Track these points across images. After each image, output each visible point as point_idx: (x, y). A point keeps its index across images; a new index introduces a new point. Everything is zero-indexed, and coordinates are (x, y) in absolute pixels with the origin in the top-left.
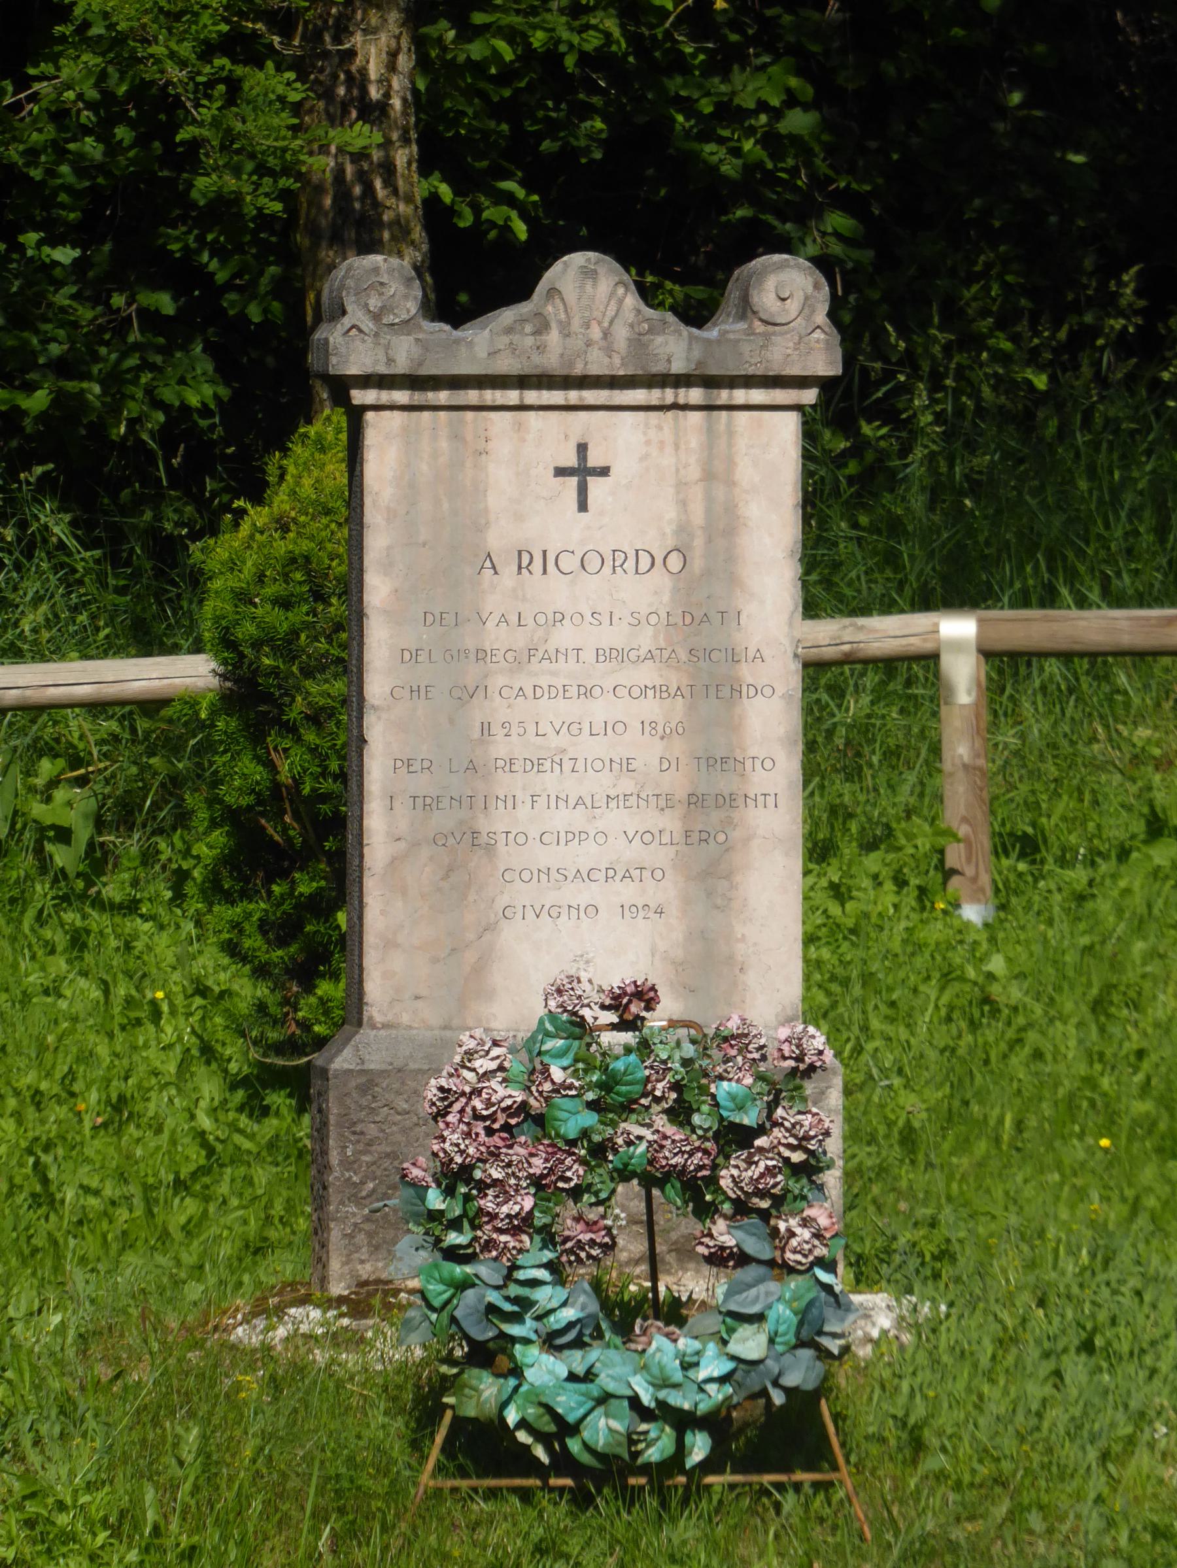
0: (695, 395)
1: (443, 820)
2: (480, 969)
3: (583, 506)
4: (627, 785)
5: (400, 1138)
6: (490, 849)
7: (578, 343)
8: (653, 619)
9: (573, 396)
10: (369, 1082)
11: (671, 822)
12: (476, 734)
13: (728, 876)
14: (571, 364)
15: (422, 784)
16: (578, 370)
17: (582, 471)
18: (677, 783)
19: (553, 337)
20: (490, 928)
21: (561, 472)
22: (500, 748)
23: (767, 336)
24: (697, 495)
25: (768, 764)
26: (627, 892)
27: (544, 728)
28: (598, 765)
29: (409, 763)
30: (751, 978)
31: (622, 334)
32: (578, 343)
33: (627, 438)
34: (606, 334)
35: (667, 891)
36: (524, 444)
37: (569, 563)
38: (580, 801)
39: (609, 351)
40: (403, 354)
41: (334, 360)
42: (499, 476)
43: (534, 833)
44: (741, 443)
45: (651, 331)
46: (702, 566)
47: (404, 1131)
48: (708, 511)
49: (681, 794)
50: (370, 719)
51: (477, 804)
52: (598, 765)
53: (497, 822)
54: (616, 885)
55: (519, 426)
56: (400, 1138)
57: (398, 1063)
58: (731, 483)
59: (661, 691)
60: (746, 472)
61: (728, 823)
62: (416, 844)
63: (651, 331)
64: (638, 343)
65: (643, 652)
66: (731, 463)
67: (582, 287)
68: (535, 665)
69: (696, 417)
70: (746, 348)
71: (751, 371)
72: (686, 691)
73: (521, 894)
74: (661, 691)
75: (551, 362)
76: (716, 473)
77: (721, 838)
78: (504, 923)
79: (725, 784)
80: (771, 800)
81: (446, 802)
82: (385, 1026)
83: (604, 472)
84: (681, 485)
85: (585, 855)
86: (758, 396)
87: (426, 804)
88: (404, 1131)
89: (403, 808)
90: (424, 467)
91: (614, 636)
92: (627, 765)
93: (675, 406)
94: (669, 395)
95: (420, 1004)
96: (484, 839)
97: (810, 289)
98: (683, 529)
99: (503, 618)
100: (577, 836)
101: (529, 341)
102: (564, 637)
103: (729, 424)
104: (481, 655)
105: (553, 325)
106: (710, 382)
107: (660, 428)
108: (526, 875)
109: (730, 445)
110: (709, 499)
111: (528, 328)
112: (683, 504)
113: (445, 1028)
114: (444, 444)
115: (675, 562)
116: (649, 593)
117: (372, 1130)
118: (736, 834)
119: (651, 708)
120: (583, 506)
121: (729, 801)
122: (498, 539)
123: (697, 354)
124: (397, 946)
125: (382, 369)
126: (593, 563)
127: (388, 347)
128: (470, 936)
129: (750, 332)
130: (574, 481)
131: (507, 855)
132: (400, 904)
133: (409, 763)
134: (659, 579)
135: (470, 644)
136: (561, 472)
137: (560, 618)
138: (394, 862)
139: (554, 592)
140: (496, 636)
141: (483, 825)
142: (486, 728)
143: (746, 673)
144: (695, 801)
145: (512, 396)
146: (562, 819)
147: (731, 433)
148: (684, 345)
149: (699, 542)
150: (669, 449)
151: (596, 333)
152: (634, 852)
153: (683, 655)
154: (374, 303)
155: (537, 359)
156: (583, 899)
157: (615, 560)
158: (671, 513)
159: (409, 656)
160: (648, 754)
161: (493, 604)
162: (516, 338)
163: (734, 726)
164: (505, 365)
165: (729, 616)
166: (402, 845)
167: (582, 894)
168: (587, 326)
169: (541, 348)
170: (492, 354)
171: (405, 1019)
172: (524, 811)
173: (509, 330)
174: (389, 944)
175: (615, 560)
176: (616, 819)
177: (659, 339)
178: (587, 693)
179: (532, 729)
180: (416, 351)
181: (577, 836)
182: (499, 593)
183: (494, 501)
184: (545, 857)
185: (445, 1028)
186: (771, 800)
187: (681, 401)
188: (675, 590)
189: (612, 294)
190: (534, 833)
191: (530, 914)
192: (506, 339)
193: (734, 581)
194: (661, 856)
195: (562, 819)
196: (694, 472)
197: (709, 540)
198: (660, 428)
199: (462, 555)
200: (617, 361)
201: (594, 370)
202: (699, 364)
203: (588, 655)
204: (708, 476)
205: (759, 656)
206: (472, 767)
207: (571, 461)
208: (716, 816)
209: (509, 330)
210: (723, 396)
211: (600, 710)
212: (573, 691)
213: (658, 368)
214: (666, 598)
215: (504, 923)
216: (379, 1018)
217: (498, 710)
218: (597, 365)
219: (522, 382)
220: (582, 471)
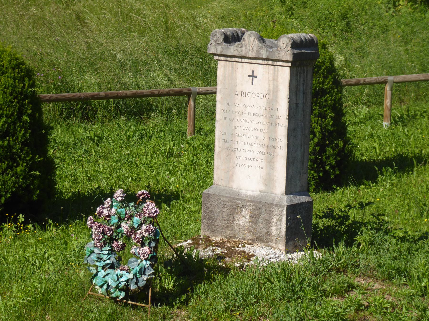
0: (270, 62)
1: (227, 145)
2: (232, 176)
3: (252, 84)
4: (257, 142)
5: (213, 208)
6: (235, 151)
7: (247, 50)
8: (263, 108)
9: (250, 61)
10: (209, 196)
11: (264, 150)
12: (233, 128)
13: (273, 163)
14: (246, 54)
15: (224, 137)
16: (248, 56)
17: (253, 76)
18: (266, 142)
19: (244, 48)
20: (234, 168)
21: (249, 76)
22: (237, 131)
23: (280, 51)
24: (271, 83)
25: (281, 140)
26: (256, 163)
27: (244, 128)
28: (253, 137)
29: (222, 132)
30: (277, 184)
31: (255, 49)
32: (247, 50)
33: (260, 69)
34: (252, 49)
35: (263, 164)
36: (244, 69)
37: (250, 95)
38: (249, 144)
39: (253, 52)
40: (219, 50)
41: (208, 50)
42: (239, 75)
43: (242, 150)
44: (280, 73)
45: (260, 49)
46: (271, 97)
47: (214, 206)
48: (273, 87)
49: (266, 145)
50: (216, 123)
51: (233, 142)
52: (253, 137)
53: (236, 146)
54: (255, 162)
55: (243, 66)
56: (213, 208)
57: (214, 193)
58: (277, 81)
59: (263, 123)
60: (280, 80)
61: (274, 152)
62: (223, 149)
63: (260, 49)
64: (258, 51)
65: (261, 115)
66: (278, 77)
67: (249, 38)
68: (243, 115)
69: (272, 67)
70: (276, 54)
71: (277, 58)
72: (268, 123)
73: (239, 161)
74: (263, 123)
75: (243, 54)
76: (275, 79)
77: (273, 155)
78: (236, 167)
79: (274, 144)
80: (281, 148)
81: (228, 141)
82: (217, 185)
83: (256, 77)
84: (269, 81)
85: (250, 155)
86: (281, 64)
87: (225, 141)
88: (214, 206)
89: (221, 141)
90: (227, 73)
91: (256, 111)
92: (258, 138)
93: (267, 64)
94: (266, 62)
95: (222, 181)
96: (234, 149)
97: (288, 42)
98: (269, 90)
99: (238, 105)
100: (249, 151)
101: (240, 49)
102: (248, 110)
103: (278, 69)
104: (235, 112)
105: (244, 46)
106: (273, 60)
107: (266, 69)
108: (240, 158)
109: (278, 73)
110: (274, 84)
111: (240, 46)
112: (269, 85)
113: (226, 186)
114: (230, 69)
115: (267, 96)
116: (262, 103)
117: (209, 206)
118: (275, 154)
119: (262, 126)
120: (252, 84)
121: (274, 147)
122: (238, 89)
123: (267, 54)
124: (219, 169)
125: (216, 53)
126: (254, 96)
127: (217, 48)
128: (231, 169)
129: (277, 50)
130: (251, 78)
131: (238, 153)
132: (220, 161)
133: (222, 132)
134: (264, 100)
135: (233, 110)
136: (249, 76)
137: (247, 106)
138: (219, 152)
139: (247, 100)
140: (238, 109)
141: (234, 146)
142: (235, 127)
143: (278, 121)
144: (269, 146)
145: (240, 60)
146: (246, 147)
147: (278, 71)
148: (265, 52)
149: (271, 93)
150: (267, 73)
151: (251, 48)
152: (258, 156)
153: (268, 116)
154: (215, 39)
155: (241, 53)
156: (249, 164)
157: (257, 95)
158: (267, 87)
159: (223, 111)
160: (261, 135)
161: (237, 102)
162: (238, 48)
163: (276, 132)
164: (236, 54)
165: (276, 109)
166: (220, 149)
167: (250, 163)
168: (249, 46)
169: (241, 51)
170: (234, 51)
171: (220, 184)
172: (240, 144)
173: (237, 46)
174: (218, 168)
175: (257, 95)
176: (255, 148)
177: (261, 50)
178: (251, 122)
179: (242, 128)
180: (221, 49)
181: (249, 151)
182: (238, 100)
183: (238, 81)
184: (243, 154)
185: (226, 186)
186: (281, 148)
187: (243, 61)
188: (267, 102)
189: (254, 40)
190: (242, 150)
191: (241, 166)
192: (236, 48)
193: (277, 102)
194: (263, 157)
195: (246, 147)
196: (271, 79)
197: (273, 93)
198: (266, 69)
199: (233, 92)
200: (254, 54)
201: (250, 56)
202: (268, 56)
203: (252, 114)
204: (274, 80)
205: (280, 118)
206: (232, 135)
207: (251, 74)
208: (272, 150)
209: (237, 46)
210: (275, 63)
211: (254, 126)
212: (249, 121)
213: (261, 57)
214: (265, 104)
215: (236, 167)
216: (215, 183)
217: (237, 123)
218: (251, 55)
219: (241, 57)
220: (253, 76)
